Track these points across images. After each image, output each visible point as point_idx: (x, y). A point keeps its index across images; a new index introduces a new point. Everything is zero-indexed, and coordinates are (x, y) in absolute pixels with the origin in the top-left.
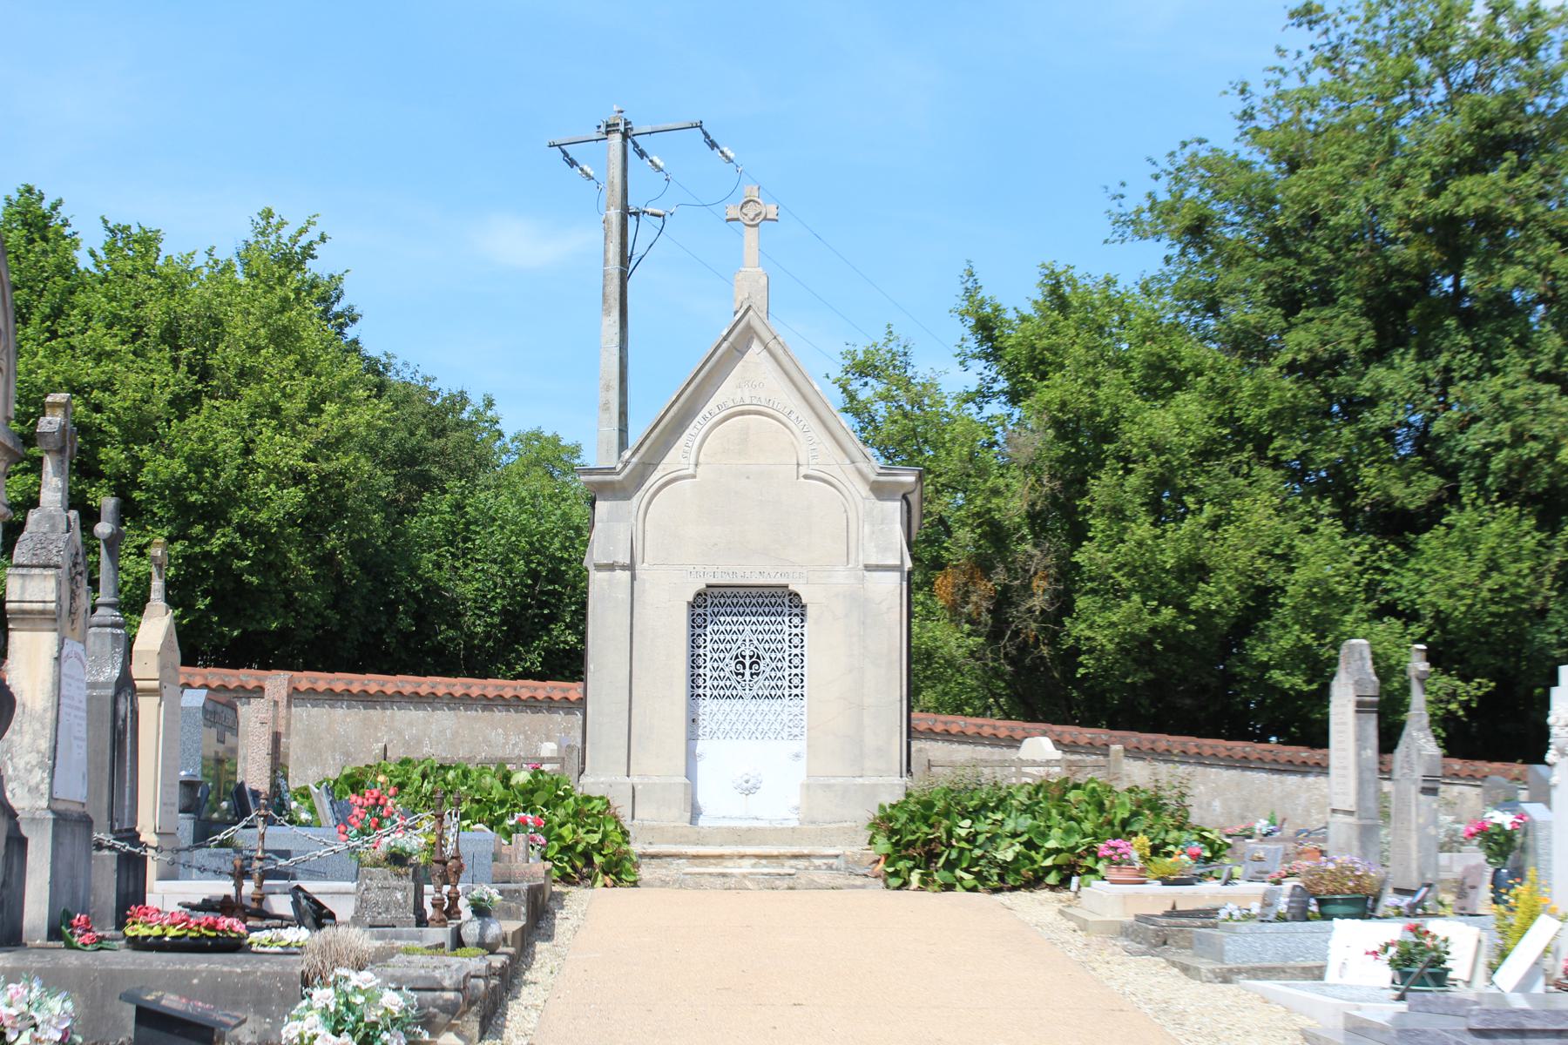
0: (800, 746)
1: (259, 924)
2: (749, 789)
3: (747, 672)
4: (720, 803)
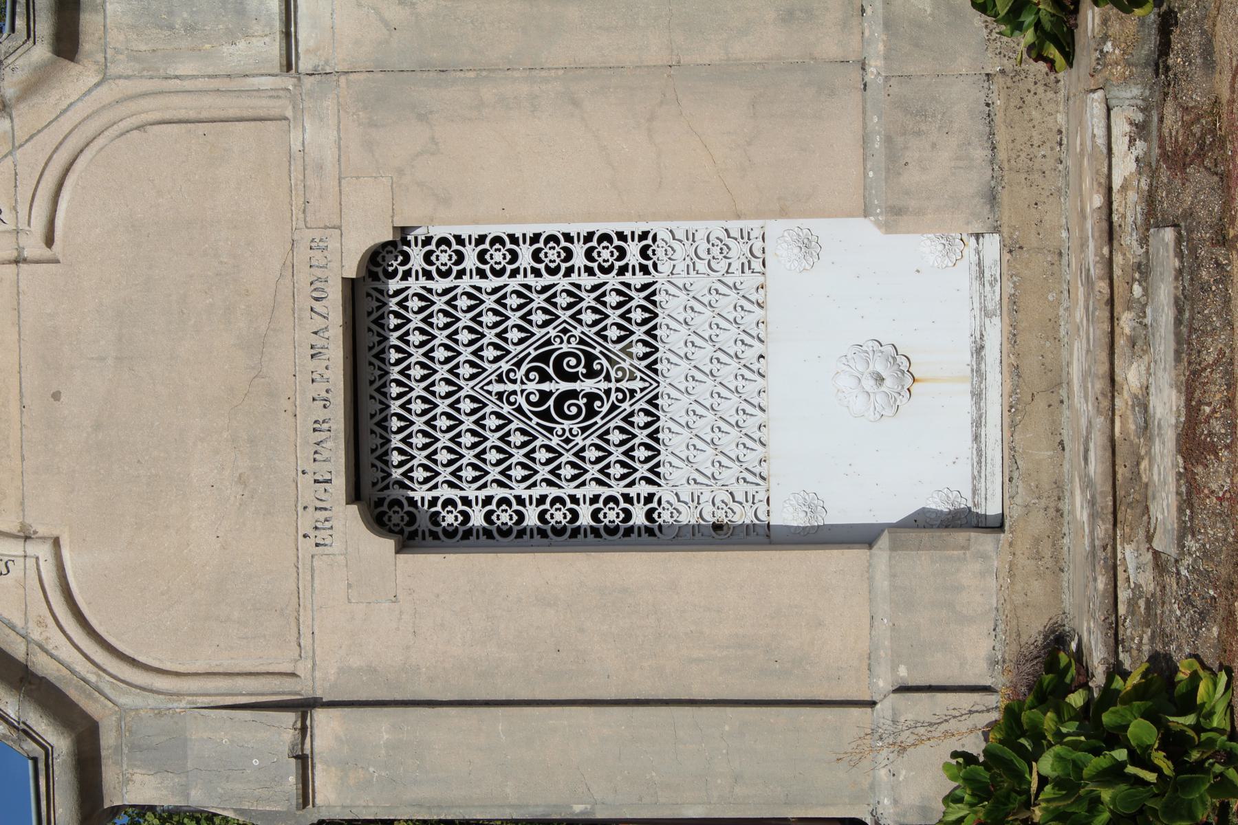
0: (779, 234)
2: (897, 373)
3: (588, 385)
4: (935, 453)
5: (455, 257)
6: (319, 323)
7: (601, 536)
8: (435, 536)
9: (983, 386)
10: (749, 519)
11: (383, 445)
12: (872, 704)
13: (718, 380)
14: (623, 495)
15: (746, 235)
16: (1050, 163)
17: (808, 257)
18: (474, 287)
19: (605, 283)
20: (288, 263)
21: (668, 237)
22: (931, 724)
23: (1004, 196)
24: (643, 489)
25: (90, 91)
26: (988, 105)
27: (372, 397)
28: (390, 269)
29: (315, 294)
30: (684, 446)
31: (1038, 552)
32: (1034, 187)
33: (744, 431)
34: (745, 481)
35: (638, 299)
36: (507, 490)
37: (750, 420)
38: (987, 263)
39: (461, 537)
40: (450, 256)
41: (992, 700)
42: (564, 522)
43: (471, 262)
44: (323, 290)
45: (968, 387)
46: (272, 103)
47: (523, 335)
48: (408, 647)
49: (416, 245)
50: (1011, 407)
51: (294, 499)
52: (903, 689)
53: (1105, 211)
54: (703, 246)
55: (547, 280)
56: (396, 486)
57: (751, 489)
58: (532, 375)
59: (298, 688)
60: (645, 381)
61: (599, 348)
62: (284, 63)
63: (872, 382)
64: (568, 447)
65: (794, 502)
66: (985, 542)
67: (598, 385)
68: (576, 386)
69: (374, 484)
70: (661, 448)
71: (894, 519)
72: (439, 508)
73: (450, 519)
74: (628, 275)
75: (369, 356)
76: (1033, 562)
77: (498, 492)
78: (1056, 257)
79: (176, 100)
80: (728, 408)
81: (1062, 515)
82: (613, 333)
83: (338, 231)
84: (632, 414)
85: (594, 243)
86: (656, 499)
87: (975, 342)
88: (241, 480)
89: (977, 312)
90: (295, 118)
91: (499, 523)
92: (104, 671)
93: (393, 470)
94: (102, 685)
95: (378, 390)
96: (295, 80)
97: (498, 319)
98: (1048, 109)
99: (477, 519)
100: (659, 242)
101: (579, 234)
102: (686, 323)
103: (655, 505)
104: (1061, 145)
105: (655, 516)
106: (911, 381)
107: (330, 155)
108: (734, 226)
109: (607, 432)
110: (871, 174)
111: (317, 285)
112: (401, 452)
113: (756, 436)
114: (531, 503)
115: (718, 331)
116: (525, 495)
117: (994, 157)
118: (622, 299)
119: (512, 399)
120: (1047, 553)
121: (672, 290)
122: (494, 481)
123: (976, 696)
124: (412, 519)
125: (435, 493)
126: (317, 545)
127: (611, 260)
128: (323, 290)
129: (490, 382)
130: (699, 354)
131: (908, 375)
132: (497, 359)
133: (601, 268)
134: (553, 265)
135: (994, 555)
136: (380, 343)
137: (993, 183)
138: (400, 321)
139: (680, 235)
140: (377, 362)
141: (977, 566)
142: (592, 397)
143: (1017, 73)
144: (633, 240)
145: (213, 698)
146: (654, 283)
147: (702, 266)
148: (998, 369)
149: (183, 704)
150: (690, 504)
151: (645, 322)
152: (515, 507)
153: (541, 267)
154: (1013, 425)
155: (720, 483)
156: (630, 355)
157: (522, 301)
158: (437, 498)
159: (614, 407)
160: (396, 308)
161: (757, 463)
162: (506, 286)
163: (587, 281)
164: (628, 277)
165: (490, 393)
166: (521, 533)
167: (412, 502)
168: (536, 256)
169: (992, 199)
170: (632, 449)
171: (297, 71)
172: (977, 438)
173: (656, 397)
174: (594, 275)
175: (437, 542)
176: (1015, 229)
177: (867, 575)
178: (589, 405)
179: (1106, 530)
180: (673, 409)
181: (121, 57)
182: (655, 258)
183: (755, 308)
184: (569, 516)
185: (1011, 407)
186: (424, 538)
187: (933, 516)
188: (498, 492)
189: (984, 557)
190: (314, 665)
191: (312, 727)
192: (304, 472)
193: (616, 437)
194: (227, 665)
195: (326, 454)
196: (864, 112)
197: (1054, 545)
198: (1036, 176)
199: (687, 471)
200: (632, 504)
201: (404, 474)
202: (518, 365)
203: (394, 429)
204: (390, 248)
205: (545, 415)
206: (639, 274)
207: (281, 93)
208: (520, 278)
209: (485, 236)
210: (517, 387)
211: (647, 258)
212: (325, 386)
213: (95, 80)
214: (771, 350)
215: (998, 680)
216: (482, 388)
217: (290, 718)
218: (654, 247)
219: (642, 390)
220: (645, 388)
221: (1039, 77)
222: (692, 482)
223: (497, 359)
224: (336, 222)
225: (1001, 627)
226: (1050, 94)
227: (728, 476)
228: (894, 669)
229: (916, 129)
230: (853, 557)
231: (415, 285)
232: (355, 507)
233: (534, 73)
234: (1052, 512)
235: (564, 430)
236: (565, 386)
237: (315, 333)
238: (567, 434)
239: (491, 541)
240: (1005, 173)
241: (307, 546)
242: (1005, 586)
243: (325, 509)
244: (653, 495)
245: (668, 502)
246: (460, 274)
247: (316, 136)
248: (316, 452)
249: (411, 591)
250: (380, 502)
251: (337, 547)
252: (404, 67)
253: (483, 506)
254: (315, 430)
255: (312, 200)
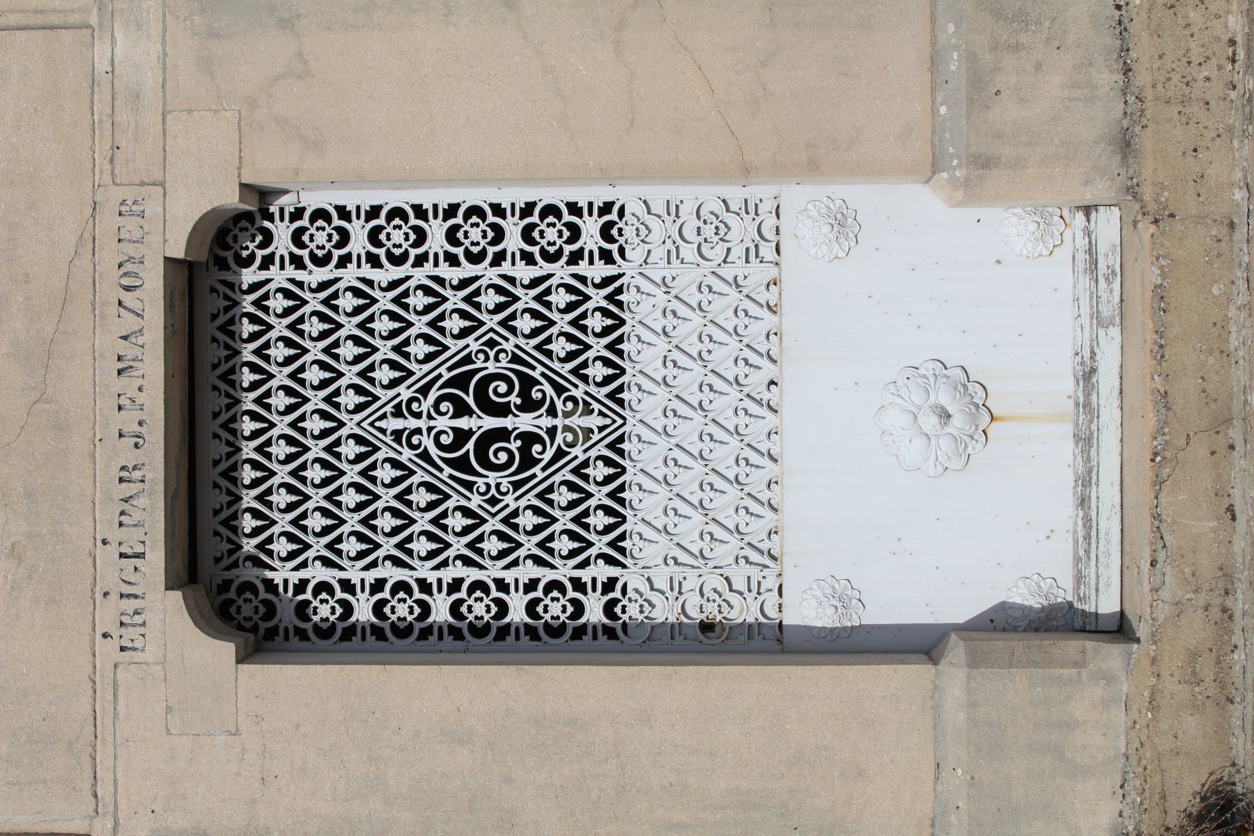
0: (803, 204)
1: (1095, 447)
2: (968, 408)
3: (525, 422)
4: (1016, 527)
5: (336, 237)
6: (130, 322)
7: (539, 639)
8: (302, 634)
9: (1094, 427)
13: (711, 416)
14: (572, 580)
15: (751, 208)
16: (1217, 88)
17: (842, 240)
18: (363, 280)
19: (550, 276)
20: (88, 236)
21: (640, 210)
23: (1146, 141)
24: (602, 571)
26: (1118, 7)
27: (216, 436)
28: (245, 253)
29: (126, 281)
31: (1194, 673)
32: (1192, 125)
35: (598, 298)
36: (406, 572)
37: (756, 474)
39: (340, 639)
40: (330, 236)
43: (359, 243)
44: (136, 275)
45: (1069, 429)
47: (432, 349)
48: (253, 801)
49: (282, 220)
50: (1156, 454)
54: (692, 224)
55: (467, 270)
57: (754, 572)
58: (444, 406)
60: (605, 416)
61: (540, 368)
63: (934, 420)
64: (493, 510)
65: (818, 593)
66: (1111, 655)
67: (537, 422)
69: (218, 560)
70: (627, 513)
71: (961, 619)
72: (308, 595)
73: (324, 611)
74: (584, 264)
75: (213, 377)
76: (1187, 688)
77: (394, 574)
78: (1225, 230)
80: (723, 457)
81: (1231, 617)
82: (560, 347)
84: (585, 464)
85: (535, 219)
86: (619, 586)
87: (1082, 363)
89: (1085, 320)
90: (101, 25)
93: (245, 540)
95: (224, 426)
97: (397, 325)
99: (363, 612)
100: (628, 217)
101: (513, 205)
103: (617, 594)
104: (1234, 61)
106: (988, 419)
107: (150, 80)
108: (736, 194)
109: (550, 489)
110: (943, 110)
111: (129, 267)
113: (763, 497)
114: (440, 590)
115: (711, 346)
116: (432, 577)
117: (1127, 83)
118: (574, 298)
120: (1208, 673)
121: (646, 286)
124: (271, 610)
126: (122, 649)
127: (559, 242)
128: (136, 275)
129: (384, 416)
131: (983, 411)
132: (394, 383)
133: (544, 254)
135: (1122, 675)
137: (1125, 123)
138: (257, 328)
139: (659, 208)
141: (1098, 692)
142: (529, 439)
146: (620, 276)
147: (688, 252)
148: (1117, 403)
150: (746, 594)
153: (459, 251)
155: (711, 564)
156: (585, 379)
157: (431, 300)
159: (560, 454)
160: (251, 309)
161: (764, 536)
163: (524, 273)
164: (582, 268)
165: (383, 431)
166: (426, 633)
167: (270, 586)
169: (1125, 145)
172: (1083, 502)
173: (621, 439)
174: (535, 264)
175: (305, 644)
176: (1163, 187)
177: (930, 703)
178: (525, 451)
180: (644, 456)
182: (622, 240)
183: (764, 313)
184: (494, 609)
185: (1156, 454)
186: (287, 638)
188: (394, 574)
189: (1109, 679)
190: (116, 824)
192: (104, 542)
195: (137, 516)
196: (933, 20)
197: (1218, 662)
198: (1196, 109)
199: (663, 545)
200: (585, 593)
201: (260, 547)
202: (424, 391)
203: (247, 482)
205: (461, 464)
208: (428, 268)
209: (380, 208)
210: (422, 423)
212: (138, 415)
214: (789, 374)
216: (372, 424)
220: (606, 427)
223: (394, 383)
224: (158, 176)
230: (908, 676)
231: (279, 277)
234: (1215, 613)
235: (488, 486)
236: (490, 423)
237: (125, 338)
238: (493, 491)
239: (382, 644)
240: (1148, 104)
242: (1142, 722)
243: (136, 597)
244: (616, 579)
245: (637, 591)
246: (344, 261)
248: (122, 513)
249: (258, 719)
250: (225, 586)
251: (152, 652)
253: (372, 594)
254: (121, 480)
255: (123, 145)
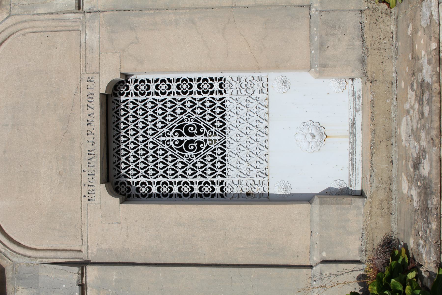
0: (274, 78)
2: (320, 134)
3: (198, 138)
4: (332, 165)
5: (146, 87)
9: (354, 139)
10: (261, 191)
11: (118, 161)
12: (311, 267)
13: (249, 136)
14: (211, 181)
18: (154, 99)
19: (205, 98)
20: (79, 87)
21: (230, 79)
22: (336, 275)
23: (369, 60)
24: (220, 179)
25: (4, 20)
26: (361, 23)
27: (114, 142)
28: (122, 92)
29: (89, 100)
30: (236, 162)
31: (381, 206)
32: (381, 56)
33: (259, 156)
34: (259, 176)
36: (166, 179)
38: (357, 90)
39: (148, 197)
40: (145, 87)
41: (361, 266)
42: (188, 192)
46: (74, 24)
48: (125, 242)
49: (132, 83)
50: (371, 146)
51: (80, 181)
52: (325, 262)
53: (438, 50)
55: (182, 96)
56: (123, 177)
57: (262, 179)
58: (176, 134)
59: (82, 257)
61: (202, 123)
62: (77, 6)
63: (311, 137)
64: (190, 162)
65: (279, 185)
66: (359, 201)
67: (202, 138)
68: (193, 138)
69: (115, 176)
70: (226, 163)
72: (139, 186)
73: (144, 190)
74: (214, 94)
75: (113, 126)
76: (380, 210)
77: (163, 180)
78: (390, 85)
79: (37, 24)
81: (391, 191)
82: (208, 117)
83: (98, 75)
84: (215, 149)
86: (224, 183)
87: (351, 122)
88: (60, 174)
89: (352, 110)
90: (82, 30)
91: (163, 192)
92: (8, 248)
93: (122, 171)
94: (7, 253)
95: (116, 139)
96: (83, 15)
98: (387, 24)
101: (195, 78)
102: (237, 114)
103: (224, 185)
104: (393, 38)
105: (224, 189)
106: (325, 137)
107: (96, 45)
110: (313, 52)
111: (90, 96)
112: (125, 163)
113: (264, 158)
114: (175, 184)
116: (173, 181)
117: (363, 44)
118: (212, 104)
119: (168, 143)
120: (385, 206)
121: (231, 100)
122: (161, 175)
123: (355, 265)
124: (129, 189)
125: (138, 180)
126: (89, 200)
128: (92, 98)
130: (242, 126)
131: (324, 135)
132: (162, 127)
134: (184, 91)
136: (117, 121)
137: (363, 55)
138: (125, 112)
139: (235, 79)
140: (116, 128)
141: (355, 212)
142: (199, 143)
143: (374, 9)
144: (216, 81)
145: (49, 260)
146: (224, 98)
147: (243, 91)
148: (361, 132)
149: (37, 262)
151: (221, 113)
152: (169, 185)
154: (372, 154)
155: (250, 177)
156: (215, 126)
158: (139, 182)
159: (208, 147)
160: (123, 107)
161: (264, 169)
162: (166, 98)
163: (198, 97)
164: (214, 95)
165: (159, 141)
166: (171, 196)
167: (129, 183)
168: (178, 87)
169: (363, 61)
170: (128, 157)
171: (83, 10)
172: (351, 160)
173: (225, 143)
176: (373, 73)
177: (309, 215)
179: (437, 200)
181: (16, 7)
182: (225, 88)
183: (264, 108)
184: (190, 189)
185: (371, 146)
186: (134, 197)
187: (334, 190)
188: (163, 180)
189: (358, 208)
190: (88, 247)
191: (86, 273)
192: (84, 171)
193: (209, 158)
194: (54, 247)
195: (93, 164)
196: (310, 27)
197: (388, 203)
198: (382, 51)
199: (236, 172)
200: (215, 185)
201: (126, 172)
202: (171, 129)
204: (122, 84)
205: (181, 150)
206: (218, 94)
207: (77, 20)
208: (172, 96)
210: (170, 138)
211: (222, 88)
213: (6, 16)
215: (364, 258)
216: (156, 139)
217: (76, 270)
218: (224, 84)
219: (219, 140)
220: (220, 139)
221: (383, 11)
222: (238, 176)
223: (162, 127)
224: (98, 71)
225: (365, 236)
226: (388, 18)
227: (253, 174)
228: (321, 253)
229: (332, 33)
230: (305, 207)
231: (131, 98)
232: (104, 185)
233: (177, 11)
234: (387, 190)
235: (188, 156)
236: (189, 138)
237: (89, 115)
238: (190, 157)
239: (159, 199)
240: (369, 50)
241: (85, 200)
243: (92, 186)
245: (229, 184)
246: (149, 94)
247: (91, 37)
248: (89, 163)
249: (126, 219)
250: (117, 183)
251: (97, 201)
252: (125, 8)
253: (157, 185)
254: (88, 154)
255: (88, 62)
